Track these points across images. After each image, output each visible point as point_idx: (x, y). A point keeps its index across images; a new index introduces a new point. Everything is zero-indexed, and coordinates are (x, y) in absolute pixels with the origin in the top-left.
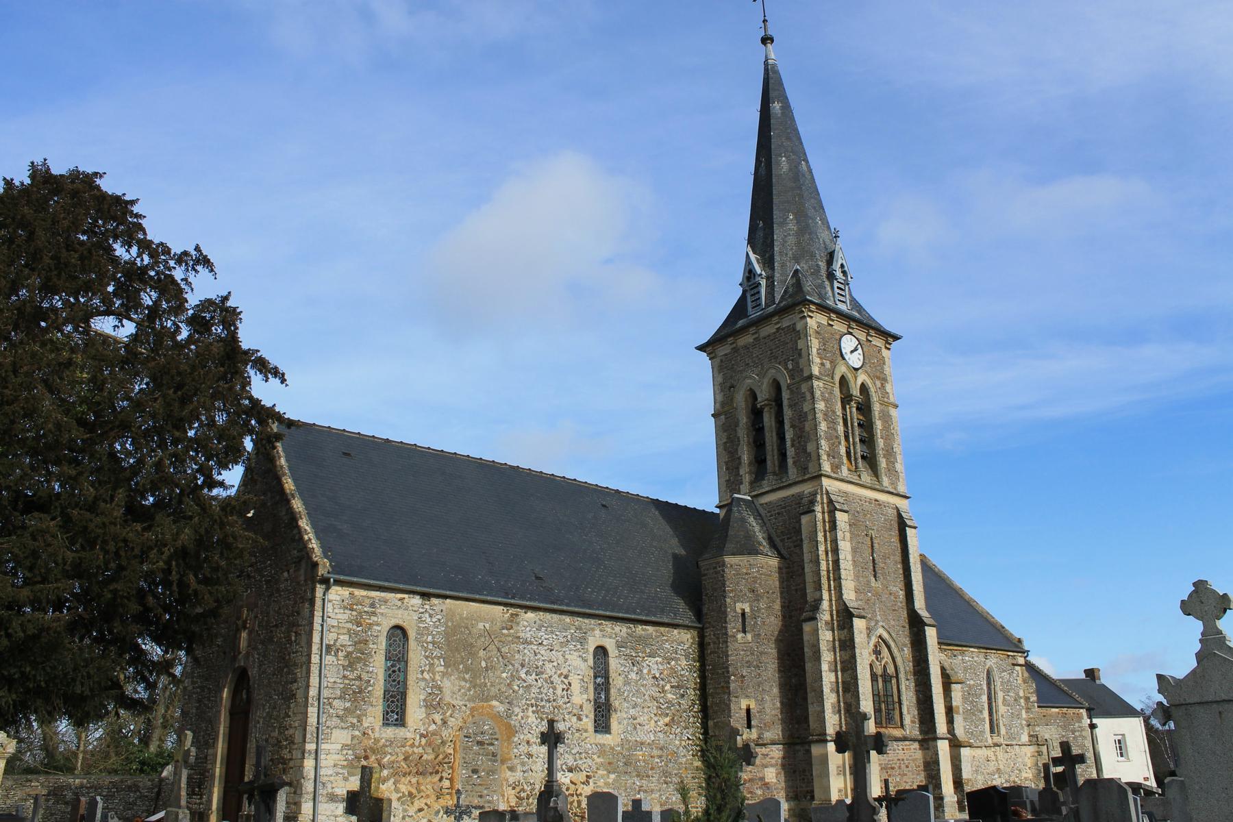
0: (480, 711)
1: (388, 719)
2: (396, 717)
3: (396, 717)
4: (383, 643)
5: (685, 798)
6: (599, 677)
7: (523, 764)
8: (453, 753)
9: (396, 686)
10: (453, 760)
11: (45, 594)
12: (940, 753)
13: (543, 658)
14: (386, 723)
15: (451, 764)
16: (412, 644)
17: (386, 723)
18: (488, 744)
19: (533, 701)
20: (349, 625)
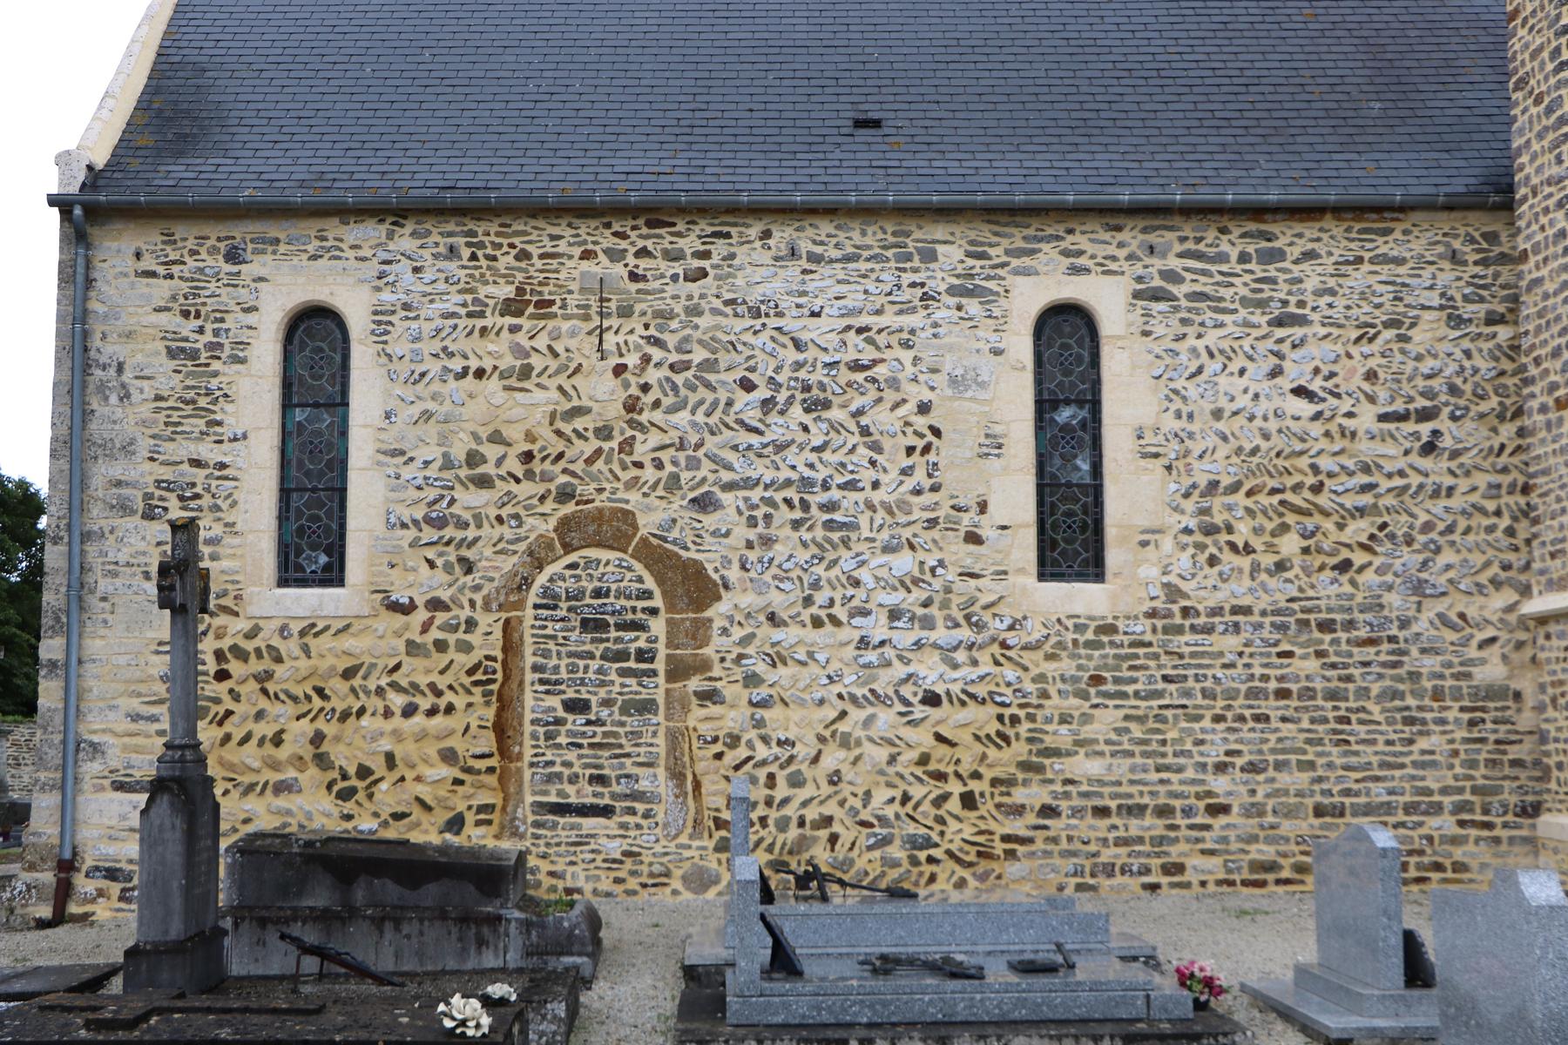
0: (591, 529)
1: (299, 568)
2: (323, 559)
3: (323, 559)
4: (266, 353)
5: (33, 834)
6: (1067, 402)
7: (752, 680)
8: (500, 657)
9: (321, 474)
10: (499, 676)
11: (626, 496)
12: (1361, 1025)
13: (828, 359)
14: (290, 573)
15: (495, 687)
16: (362, 357)
17: (290, 573)
18: (619, 627)
19: (790, 493)
20: (171, 321)
